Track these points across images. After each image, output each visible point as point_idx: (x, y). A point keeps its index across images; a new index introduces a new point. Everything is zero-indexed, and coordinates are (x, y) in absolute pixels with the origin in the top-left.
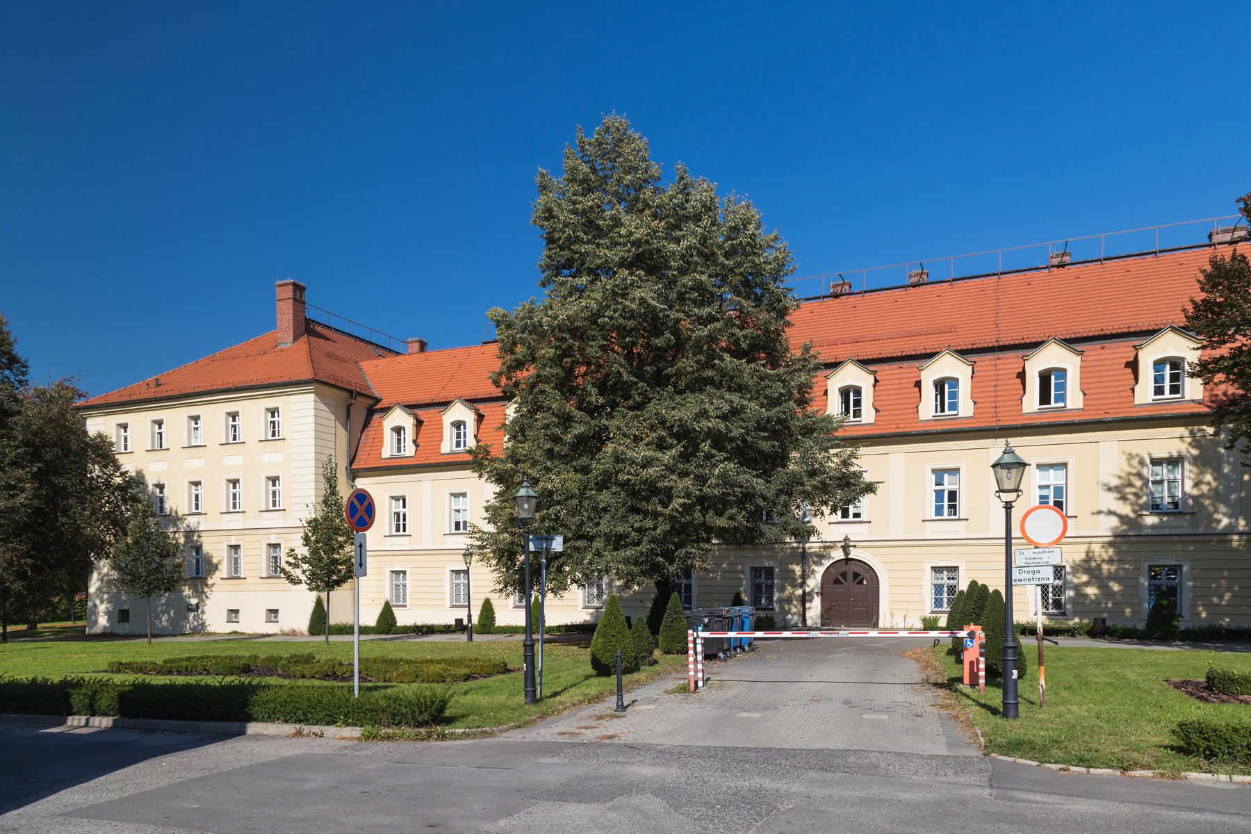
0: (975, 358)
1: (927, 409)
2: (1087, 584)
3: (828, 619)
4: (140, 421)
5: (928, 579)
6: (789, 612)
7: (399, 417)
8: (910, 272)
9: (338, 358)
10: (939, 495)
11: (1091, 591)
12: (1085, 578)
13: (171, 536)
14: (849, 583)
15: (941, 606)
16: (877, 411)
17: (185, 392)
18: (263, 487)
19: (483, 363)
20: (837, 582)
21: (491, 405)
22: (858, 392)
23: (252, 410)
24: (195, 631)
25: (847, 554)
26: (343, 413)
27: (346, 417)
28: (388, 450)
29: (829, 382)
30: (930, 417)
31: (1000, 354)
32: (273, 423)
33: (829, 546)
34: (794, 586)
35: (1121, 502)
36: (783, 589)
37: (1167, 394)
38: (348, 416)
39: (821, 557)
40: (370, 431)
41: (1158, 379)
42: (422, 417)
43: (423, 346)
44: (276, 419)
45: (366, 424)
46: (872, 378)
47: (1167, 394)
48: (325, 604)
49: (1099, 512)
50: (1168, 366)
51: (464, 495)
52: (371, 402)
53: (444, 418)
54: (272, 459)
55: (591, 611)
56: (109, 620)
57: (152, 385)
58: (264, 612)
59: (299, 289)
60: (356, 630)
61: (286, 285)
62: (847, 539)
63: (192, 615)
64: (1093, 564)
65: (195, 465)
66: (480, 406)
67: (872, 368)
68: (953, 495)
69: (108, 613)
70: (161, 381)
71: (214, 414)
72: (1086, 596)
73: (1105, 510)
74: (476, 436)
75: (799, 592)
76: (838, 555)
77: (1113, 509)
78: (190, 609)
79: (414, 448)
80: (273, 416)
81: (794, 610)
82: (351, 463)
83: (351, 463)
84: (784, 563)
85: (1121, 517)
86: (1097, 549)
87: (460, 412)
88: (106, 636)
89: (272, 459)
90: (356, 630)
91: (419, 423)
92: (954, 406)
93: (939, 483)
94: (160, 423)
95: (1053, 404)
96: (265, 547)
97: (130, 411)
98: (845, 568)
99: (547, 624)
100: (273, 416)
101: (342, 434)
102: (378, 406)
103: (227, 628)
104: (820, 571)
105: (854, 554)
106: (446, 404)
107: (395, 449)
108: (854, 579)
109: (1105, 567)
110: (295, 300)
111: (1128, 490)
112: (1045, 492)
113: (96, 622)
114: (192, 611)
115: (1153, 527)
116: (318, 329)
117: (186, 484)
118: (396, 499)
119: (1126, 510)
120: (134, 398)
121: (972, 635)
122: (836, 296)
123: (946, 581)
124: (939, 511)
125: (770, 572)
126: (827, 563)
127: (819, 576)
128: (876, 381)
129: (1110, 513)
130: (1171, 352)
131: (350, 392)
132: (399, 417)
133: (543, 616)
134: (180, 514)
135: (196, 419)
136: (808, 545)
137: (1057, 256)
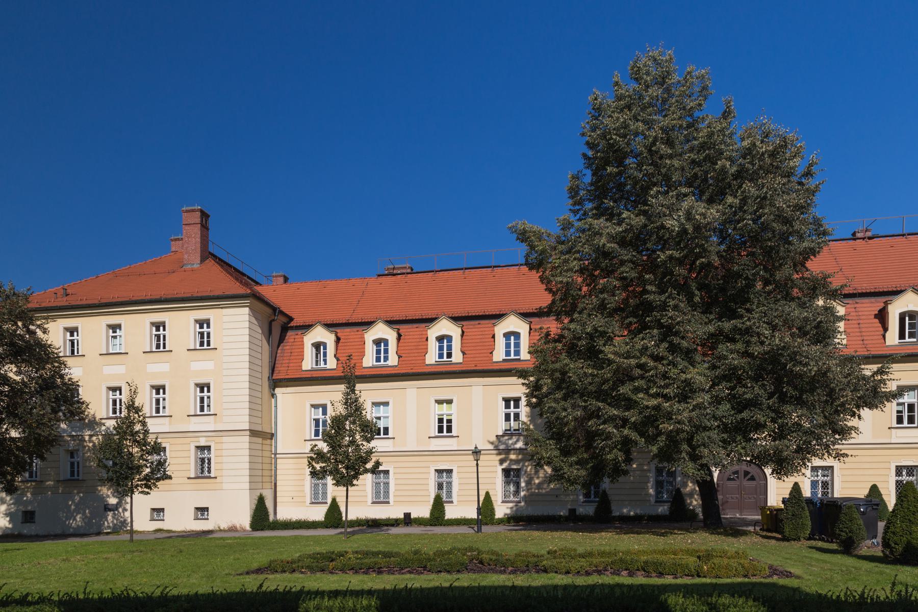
0: (464, 323)
1: (432, 357)
4: (93, 328)
13: (87, 438)
16: (400, 357)
17: (103, 301)
18: (192, 396)
23: (181, 324)
24: (116, 530)
27: (269, 333)
28: (308, 363)
30: (433, 362)
32: (72, 342)
37: (445, 359)
40: (286, 346)
41: (508, 346)
43: (286, 280)
44: (75, 337)
45: (282, 340)
46: (460, 330)
47: (445, 359)
48: (343, 509)
50: (512, 338)
51: (450, 402)
52: (284, 320)
53: (366, 336)
54: (202, 367)
55: (511, 505)
58: (193, 510)
59: (204, 215)
61: (193, 211)
63: (110, 514)
70: (69, 291)
78: (107, 508)
79: (461, 354)
80: (72, 335)
81: (695, 503)
89: (202, 367)
92: (449, 355)
95: (907, 340)
96: (193, 449)
99: (497, 517)
100: (72, 335)
102: (292, 324)
103: (152, 526)
106: (369, 324)
108: (745, 476)
110: (202, 225)
114: (110, 510)
117: (104, 390)
118: (315, 406)
120: (43, 305)
123: (820, 478)
124: (440, 430)
128: (463, 332)
130: (319, 339)
134: (98, 417)
135: (115, 328)
137: (862, 231)
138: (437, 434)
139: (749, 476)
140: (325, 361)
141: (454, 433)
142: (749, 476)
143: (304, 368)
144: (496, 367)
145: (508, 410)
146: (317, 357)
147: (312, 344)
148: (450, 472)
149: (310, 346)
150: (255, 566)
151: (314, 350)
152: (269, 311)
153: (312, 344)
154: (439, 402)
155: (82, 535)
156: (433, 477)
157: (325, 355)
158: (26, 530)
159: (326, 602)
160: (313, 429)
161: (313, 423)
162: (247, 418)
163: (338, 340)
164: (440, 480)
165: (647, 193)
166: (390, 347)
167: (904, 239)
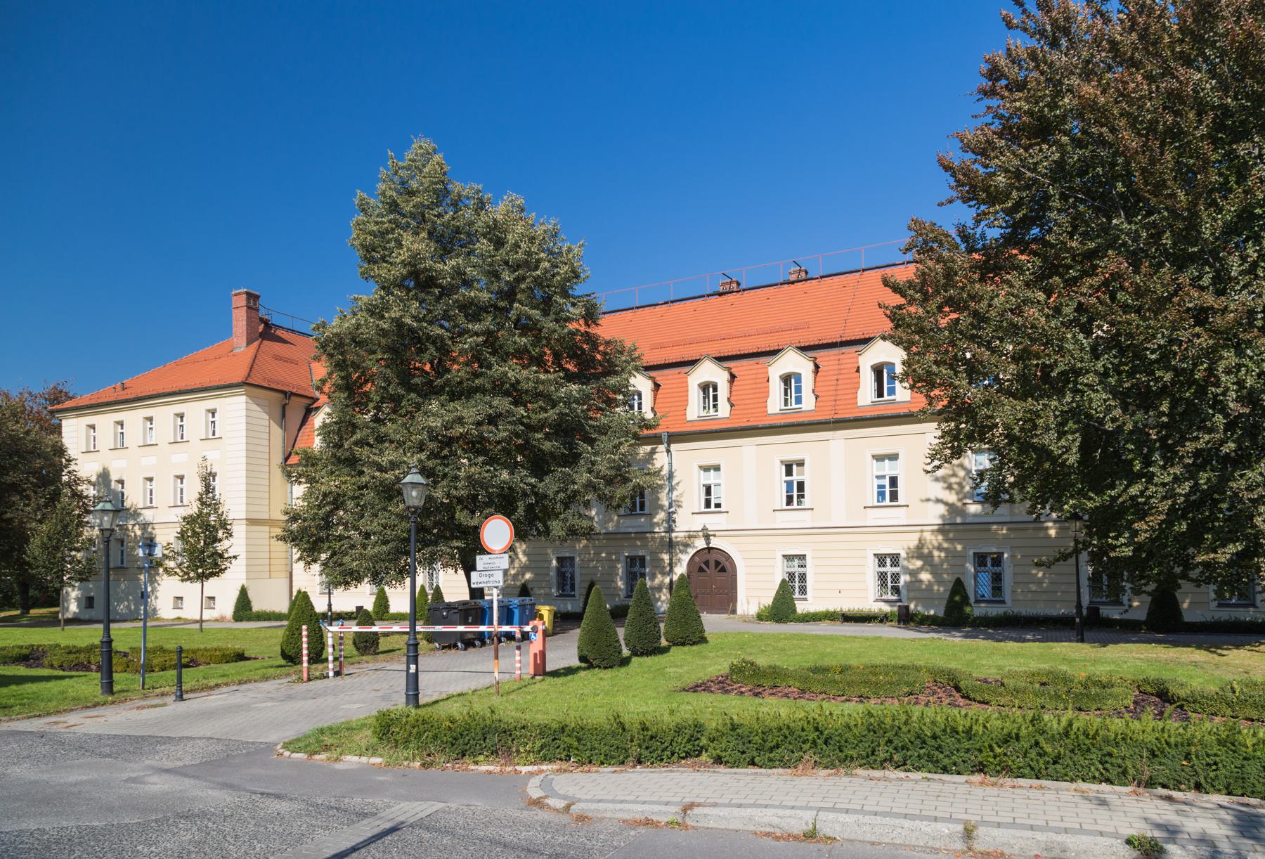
2: (921, 569)
6: (659, 599)
8: (791, 273)
9: (287, 360)
10: (789, 484)
11: (925, 577)
12: (919, 563)
14: (711, 571)
20: (701, 570)
21: (744, 362)
22: (798, 377)
23: (195, 409)
25: (708, 543)
26: (278, 412)
27: (282, 416)
29: (770, 369)
31: (844, 349)
33: (691, 536)
34: (663, 574)
35: (947, 492)
36: (653, 577)
38: (284, 415)
39: (687, 545)
49: (928, 500)
51: (717, 468)
52: (308, 401)
56: (78, 606)
57: (119, 389)
59: (252, 297)
62: (704, 529)
64: (926, 551)
65: (148, 462)
67: (653, 374)
68: (801, 486)
69: (78, 599)
71: (164, 413)
72: (921, 581)
73: (933, 498)
74: (652, 409)
75: (667, 580)
76: (700, 544)
77: (940, 497)
79: (728, 406)
81: (663, 598)
82: (286, 459)
83: (286, 459)
84: (655, 553)
85: (946, 504)
86: (928, 536)
87: (709, 371)
88: (75, 621)
92: (799, 400)
93: (789, 472)
98: (707, 557)
101: (277, 432)
104: (685, 558)
105: (715, 543)
109: (936, 553)
110: (249, 307)
111: (953, 480)
112: (881, 482)
115: (975, 515)
116: (279, 333)
119: (952, 498)
121: (535, 629)
122: (721, 294)
125: (642, 559)
126: (692, 552)
127: (685, 563)
128: (817, 367)
129: (938, 501)
131: (284, 393)
133: (459, 603)
135: (150, 419)
136: (674, 535)
138: (703, 509)
140: (715, 406)
141: (901, 500)
143: (689, 418)
145: (789, 478)
146: (786, 394)
148: (802, 557)
149: (696, 387)
150: (690, 680)
152: (281, 396)
154: (706, 469)
156: (872, 564)
157: (798, 390)
160: (703, 497)
161: (703, 491)
162: (244, 508)
163: (657, 386)
164: (882, 569)
166: (803, 384)
167: (720, 299)
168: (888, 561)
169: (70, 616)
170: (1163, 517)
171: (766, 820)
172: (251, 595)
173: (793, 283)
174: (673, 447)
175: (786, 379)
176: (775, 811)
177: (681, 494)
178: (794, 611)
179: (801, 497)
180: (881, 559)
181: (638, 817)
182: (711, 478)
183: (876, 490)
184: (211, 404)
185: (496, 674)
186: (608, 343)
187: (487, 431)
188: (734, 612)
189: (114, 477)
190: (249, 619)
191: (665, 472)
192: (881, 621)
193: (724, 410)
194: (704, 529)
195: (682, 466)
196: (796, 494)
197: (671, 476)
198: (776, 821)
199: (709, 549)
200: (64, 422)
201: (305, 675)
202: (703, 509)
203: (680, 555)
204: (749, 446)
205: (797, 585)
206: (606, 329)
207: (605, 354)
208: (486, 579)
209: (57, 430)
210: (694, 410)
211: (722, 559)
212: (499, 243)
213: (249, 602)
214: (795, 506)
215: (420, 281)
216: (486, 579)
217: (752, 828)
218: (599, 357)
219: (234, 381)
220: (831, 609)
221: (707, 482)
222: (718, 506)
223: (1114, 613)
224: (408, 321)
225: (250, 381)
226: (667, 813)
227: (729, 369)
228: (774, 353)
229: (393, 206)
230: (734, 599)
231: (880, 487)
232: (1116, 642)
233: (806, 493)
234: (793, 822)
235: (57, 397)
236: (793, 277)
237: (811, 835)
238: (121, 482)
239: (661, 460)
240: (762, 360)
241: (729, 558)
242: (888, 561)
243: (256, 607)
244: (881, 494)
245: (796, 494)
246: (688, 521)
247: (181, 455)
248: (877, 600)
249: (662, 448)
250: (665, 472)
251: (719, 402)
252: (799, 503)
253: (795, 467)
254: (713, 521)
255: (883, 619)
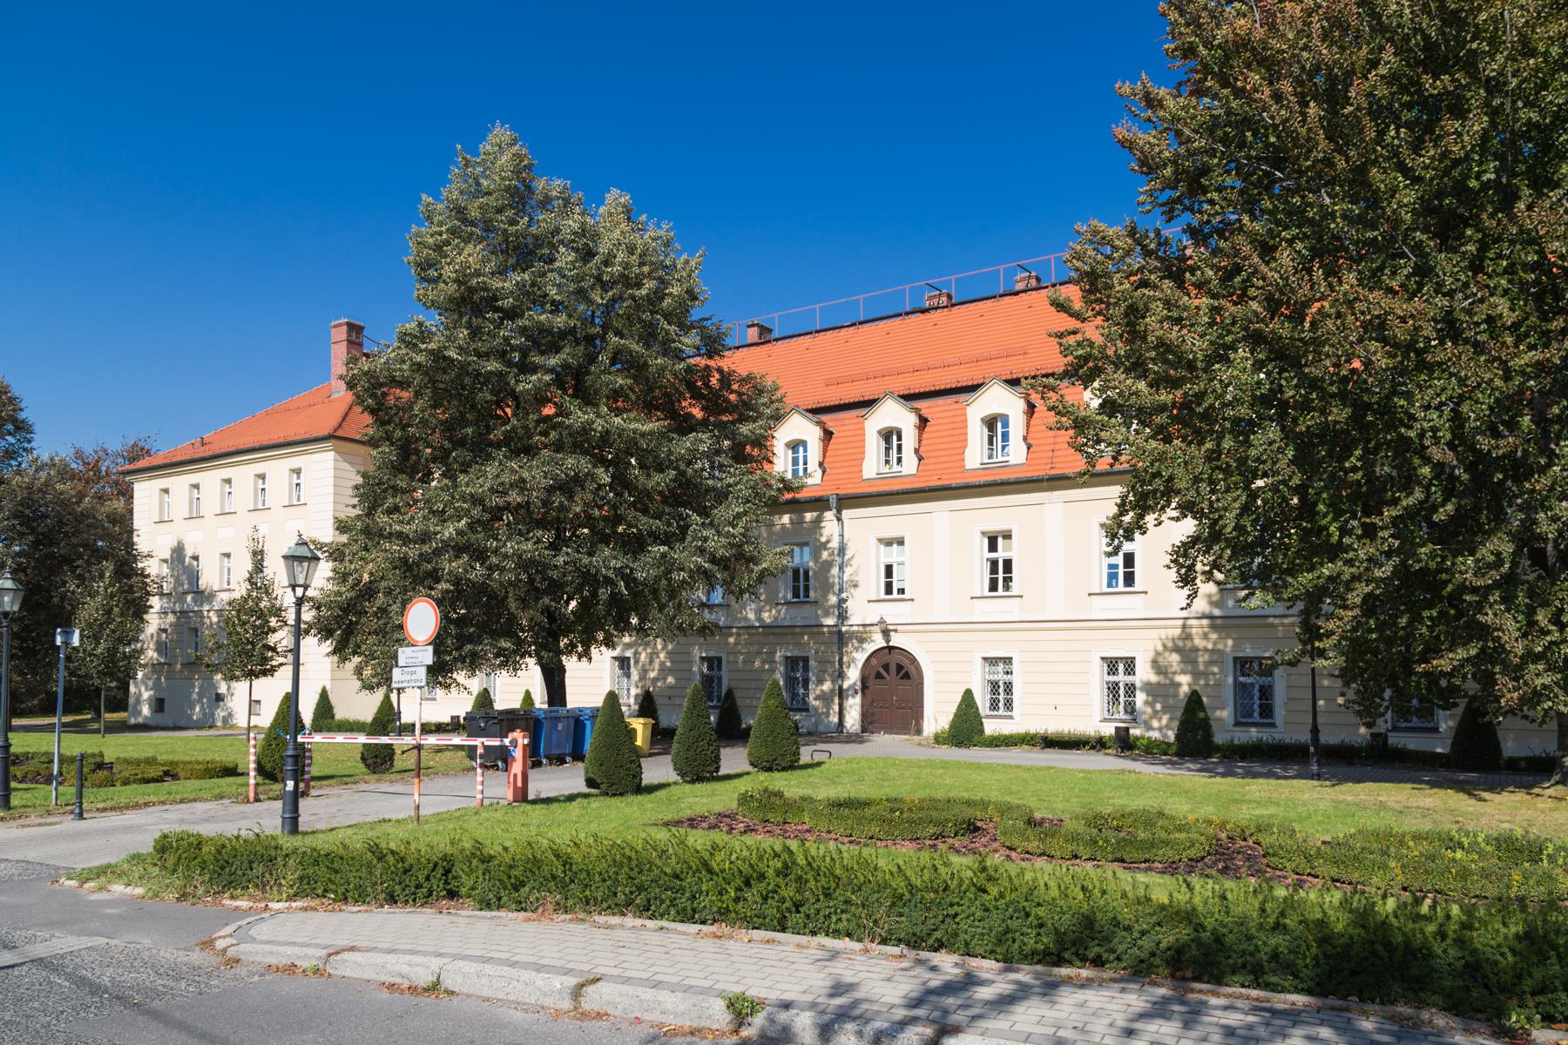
3: (870, 722)
5: (1097, 677)
7: (798, 427)
10: (994, 563)
15: (1251, 715)
19: (1032, 327)
20: (879, 676)
21: (940, 401)
23: (277, 468)
25: (888, 641)
39: (862, 641)
42: (831, 426)
51: (901, 542)
59: (354, 329)
60: (418, 727)
62: (882, 621)
66: (923, 405)
68: (1008, 565)
71: (243, 473)
74: (821, 464)
76: (878, 642)
90: (418, 727)
91: (828, 435)
93: (993, 547)
94: (298, 472)
97: (171, 475)
98: (888, 658)
105: (896, 641)
107: (986, 452)
110: (350, 342)
113: (140, 713)
122: (924, 311)
132: (798, 427)
139: (883, 672)
140: (899, 460)
141: (1138, 586)
142: (883, 672)
143: (969, 465)
144: (1012, 477)
145: (993, 555)
147: (879, 432)
148: (1008, 661)
149: (875, 435)
151: (986, 431)
153: (879, 432)
154: (888, 543)
155: (199, 728)
157: (1005, 437)
158: (161, 719)
159: (154, 799)
160: (883, 580)
161: (987, 567)
163: (923, 422)
165: (1440, 94)
166: (1011, 429)
168: (1121, 668)
169: (140, 720)
170: (1356, 612)
171: (396, 968)
172: (333, 700)
173: (1016, 294)
174: (846, 513)
175: (990, 423)
176: (408, 957)
177: (856, 573)
178: (982, 731)
179: (1007, 580)
180: (1112, 664)
181: (274, 961)
182: (893, 555)
183: (1105, 571)
184: (295, 462)
185: (416, 797)
186: (749, 379)
187: (586, 489)
188: (919, 732)
189: (189, 552)
190: (329, 730)
191: (834, 544)
192: (1093, 748)
193: (910, 465)
194: (882, 621)
195: (858, 537)
196: (1000, 575)
197: (842, 550)
198: (405, 969)
199: (890, 648)
200: (136, 486)
201: (252, 795)
202: (883, 596)
203: (855, 655)
204: (940, 510)
205: (1001, 697)
206: (739, 362)
207: (740, 394)
208: (408, 677)
209: (127, 494)
210: (872, 466)
211: (905, 662)
212: (588, 254)
213: (330, 708)
214: (1000, 591)
215: (470, 303)
216: (408, 677)
217: (383, 978)
218: (733, 397)
219: (321, 434)
220: (1032, 731)
221: (889, 561)
222: (901, 591)
223: (1412, 742)
224: (452, 354)
225: (340, 433)
226: (307, 958)
227: (917, 411)
228: (973, 388)
229: (460, 212)
230: (918, 714)
231: (1111, 566)
232: (1358, 781)
233: (1015, 575)
234: (421, 971)
235: (136, 452)
236: (1020, 286)
237: (434, 988)
238: (196, 558)
239: (830, 526)
240: (962, 397)
241: (913, 660)
242: (1121, 668)
243: (340, 714)
244: (1112, 577)
245: (1000, 575)
246: (863, 608)
247: (246, 520)
248: (1105, 720)
249: (829, 515)
250: (834, 544)
251: (904, 455)
252: (1007, 588)
253: (1000, 540)
254: (893, 612)
255: (1099, 744)
